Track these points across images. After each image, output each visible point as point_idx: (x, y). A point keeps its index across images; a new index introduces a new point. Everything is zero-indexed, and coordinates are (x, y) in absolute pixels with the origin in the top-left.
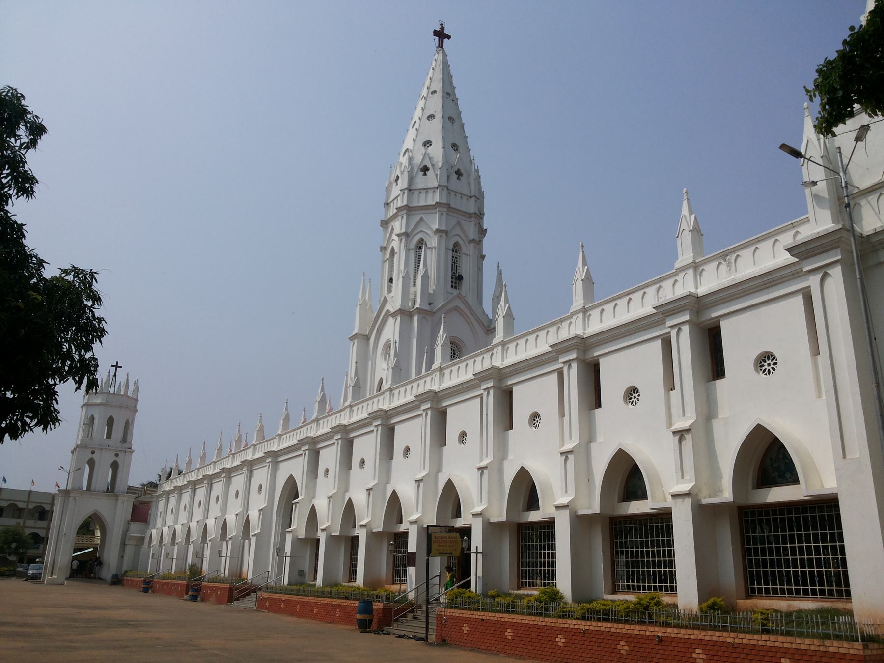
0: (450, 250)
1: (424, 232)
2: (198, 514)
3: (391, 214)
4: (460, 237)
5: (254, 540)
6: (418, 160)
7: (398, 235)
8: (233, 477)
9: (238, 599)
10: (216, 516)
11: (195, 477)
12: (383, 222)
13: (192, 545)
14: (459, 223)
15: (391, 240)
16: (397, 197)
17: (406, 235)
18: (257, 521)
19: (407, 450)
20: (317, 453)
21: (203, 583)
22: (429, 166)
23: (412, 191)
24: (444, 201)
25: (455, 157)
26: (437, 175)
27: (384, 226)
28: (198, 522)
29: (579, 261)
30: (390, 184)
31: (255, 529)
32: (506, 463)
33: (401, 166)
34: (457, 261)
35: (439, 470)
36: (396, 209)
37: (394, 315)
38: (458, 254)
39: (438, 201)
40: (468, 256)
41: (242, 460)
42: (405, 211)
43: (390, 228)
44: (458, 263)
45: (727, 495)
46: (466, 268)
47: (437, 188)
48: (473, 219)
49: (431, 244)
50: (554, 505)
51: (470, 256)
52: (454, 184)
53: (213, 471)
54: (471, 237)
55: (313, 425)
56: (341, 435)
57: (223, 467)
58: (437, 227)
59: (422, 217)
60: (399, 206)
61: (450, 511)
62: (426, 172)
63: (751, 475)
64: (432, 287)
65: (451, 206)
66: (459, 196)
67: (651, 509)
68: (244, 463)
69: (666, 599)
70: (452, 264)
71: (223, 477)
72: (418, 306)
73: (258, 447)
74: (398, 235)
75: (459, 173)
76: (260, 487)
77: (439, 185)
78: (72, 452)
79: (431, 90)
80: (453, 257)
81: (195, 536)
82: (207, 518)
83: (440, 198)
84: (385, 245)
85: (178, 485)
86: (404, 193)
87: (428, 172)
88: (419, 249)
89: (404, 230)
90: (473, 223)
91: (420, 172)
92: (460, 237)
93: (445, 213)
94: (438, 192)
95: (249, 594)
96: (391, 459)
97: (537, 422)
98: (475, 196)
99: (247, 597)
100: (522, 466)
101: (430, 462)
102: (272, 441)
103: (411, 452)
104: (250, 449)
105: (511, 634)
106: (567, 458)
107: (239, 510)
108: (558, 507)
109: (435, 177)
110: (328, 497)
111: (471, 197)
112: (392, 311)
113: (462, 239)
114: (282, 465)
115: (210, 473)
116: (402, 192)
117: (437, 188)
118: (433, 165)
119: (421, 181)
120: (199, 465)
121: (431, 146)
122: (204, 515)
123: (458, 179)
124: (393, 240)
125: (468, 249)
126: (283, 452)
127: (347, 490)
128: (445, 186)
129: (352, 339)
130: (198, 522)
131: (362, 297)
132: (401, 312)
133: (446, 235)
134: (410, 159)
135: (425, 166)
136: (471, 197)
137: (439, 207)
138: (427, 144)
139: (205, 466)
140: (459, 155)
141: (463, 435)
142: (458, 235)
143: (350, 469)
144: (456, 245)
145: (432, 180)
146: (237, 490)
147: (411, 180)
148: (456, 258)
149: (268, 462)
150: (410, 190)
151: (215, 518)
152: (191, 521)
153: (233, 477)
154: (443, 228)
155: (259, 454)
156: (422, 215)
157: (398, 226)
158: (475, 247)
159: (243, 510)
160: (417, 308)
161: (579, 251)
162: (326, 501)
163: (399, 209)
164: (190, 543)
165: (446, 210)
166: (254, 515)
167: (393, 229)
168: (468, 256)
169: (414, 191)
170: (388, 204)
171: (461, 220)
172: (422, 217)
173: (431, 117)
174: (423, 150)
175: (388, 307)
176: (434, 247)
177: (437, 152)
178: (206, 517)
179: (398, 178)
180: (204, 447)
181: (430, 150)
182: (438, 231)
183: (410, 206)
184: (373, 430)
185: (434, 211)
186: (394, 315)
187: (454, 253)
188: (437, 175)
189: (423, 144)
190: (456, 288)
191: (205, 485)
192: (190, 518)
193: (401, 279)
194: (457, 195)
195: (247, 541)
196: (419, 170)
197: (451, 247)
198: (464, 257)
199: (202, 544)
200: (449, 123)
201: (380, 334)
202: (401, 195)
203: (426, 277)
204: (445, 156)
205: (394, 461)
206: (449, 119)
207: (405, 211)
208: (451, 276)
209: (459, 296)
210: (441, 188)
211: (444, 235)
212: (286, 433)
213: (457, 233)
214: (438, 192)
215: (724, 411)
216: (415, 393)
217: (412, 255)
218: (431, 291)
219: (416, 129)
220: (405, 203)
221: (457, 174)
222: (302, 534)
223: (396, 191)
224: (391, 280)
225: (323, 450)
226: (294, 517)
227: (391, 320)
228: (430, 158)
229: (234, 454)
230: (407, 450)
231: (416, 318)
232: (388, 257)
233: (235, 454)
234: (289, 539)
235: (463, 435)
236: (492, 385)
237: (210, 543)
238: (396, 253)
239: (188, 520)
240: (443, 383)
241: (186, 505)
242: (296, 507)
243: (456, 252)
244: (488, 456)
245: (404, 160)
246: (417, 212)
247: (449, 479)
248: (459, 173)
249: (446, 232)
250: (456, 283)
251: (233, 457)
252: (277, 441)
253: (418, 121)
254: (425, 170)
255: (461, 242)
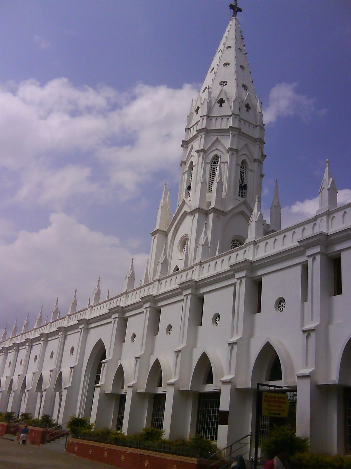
0: (239, 165)
1: (219, 150)
2: (19, 370)
3: (191, 137)
4: (247, 156)
5: (65, 393)
6: (216, 94)
7: (197, 152)
8: (68, 335)
9: (49, 442)
10: (34, 372)
11: (8, 344)
12: (184, 142)
13: (13, 393)
14: (246, 145)
15: (191, 155)
16: (197, 123)
17: (203, 151)
18: (69, 377)
19: (170, 328)
20: (158, 312)
21: (20, 425)
22: (225, 99)
23: (210, 118)
24: (236, 126)
25: (245, 96)
26: (231, 107)
27: (185, 146)
28: (19, 375)
29: (202, 234)
30: (191, 114)
31: (67, 382)
32: (252, 339)
33: (201, 100)
34: (243, 175)
35: (194, 346)
36: (196, 131)
37: (192, 213)
38: (245, 170)
39: (231, 126)
40: (253, 172)
41: (58, 326)
42: (204, 133)
43: (190, 148)
44: (244, 176)
45: (334, 377)
46: (251, 180)
47: (231, 116)
48: (258, 143)
49: (224, 160)
50: (221, 381)
51: (254, 172)
52: (245, 115)
53: (21, 340)
54: (256, 158)
55: (122, 297)
56: (118, 315)
57: (81, 318)
58: (230, 146)
59: (217, 138)
60: (198, 129)
61: (157, 382)
62: (222, 104)
63: (157, 382)
64: (224, 193)
65: (241, 131)
66: (247, 124)
67: (163, 391)
68: (60, 329)
69: (214, 443)
70: (240, 178)
71: (42, 341)
72: (213, 205)
73: (72, 316)
74: (197, 152)
75: (247, 106)
76: (72, 349)
77: (232, 114)
78: (185, 132)
79: (227, 45)
80: (241, 172)
81: (16, 386)
82: (27, 373)
83: (234, 122)
84: (185, 161)
85: (30, 338)
86: (204, 118)
87: (224, 104)
88: (214, 164)
89: (202, 148)
90: (258, 147)
91: (217, 103)
92: (247, 156)
93: (236, 136)
94: (231, 119)
95: (58, 438)
96: (123, 343)
97: (218, 320)
98: (260, 126)
99: (57, 441)
100: (268, 342)
101: (244, 330)
102: (63, 320)
103: (173, 329)
104: (65, 319)
105: (148, 463)
106: (232, 348)
107: (53, 367)
108: (300, 377)
109: (229, 107)
110: (136, 358)
111: (256, 126)
112: (189, 211)
113: (249, 158)
114: (92, 331)
115: (31, 337)
116: (202, 118)
117: (231, 116)
118: (228, 99)
119: (217, 111)
120: (23, 331)
121: (226, 85)
122: (12, 373)
123: (247, 111)
124: (192, 156)
125: (253, 166)
126: (99, 318)
127: (120, 359)
128: (237, 115)
129: (153, 234)
130: (19, 375)
131: (163, 202)
132: (198, 210)
133: (237, 154)
134: (210, 93)
135: (221, 99)
136: (256, 126)
137: (232, 130)
138: (223, 83)
139: (27, 332)
140: (248, 93)
141: (217, 317)
142: (246, 154)
143: (157, 334)
144: (244, 162)
145: (227, 109)
146: (36, 355)
147: (210, 109)
148: (243, 173)
149: (81, 329)
150: (208, 117)
151: (34, 373)
152: (27, 373)
153: (68, 335)
154: (235, 147)
155: (54, 329)
156: (218, 137)
157: (197, 145)
158: (258, 165)
159: (57, 368)
160: (213, 208)
161: (164, 247)
162: (133, 361)
163: (199, 131)
164: (12, 392)
165: (237, 133)
166: (66, 372)
167: (192, 147)
168: (253, 172)
169: (212, 118)
170: (189, 129)
171: (248, 143)
172: (217, 138)
173: (226, 64)
174: (220, 87)
175: (186, 208)
176: (226, 162)
177: (231, 90)
178: (25, 372)
179: (198, 108)
180: (57, 303)
181: (225, 87)
182: (230, 149)
183: (208, 129)
184: (143, 312)
185: (227, 134)
186: (192, 213)
187: (242, 169)
188: (231, 107)
189: (220, 83)
190: (242, 196)
191: (59, 337)
192: (13, 373)
193: (200, 184)
194: (246, 123)
195: (58, 394)
196: (217, 102)
197: (240, 163)
198: (250, 172)
199: (21, 394)
200: (240, 69)
201: (177, 231)
202: (201, 120)
203: (220, 184)
204: (238, 92)
205: (125, 344)
206: (240, 67)
207: (204, 133)
208: (239, 187)
209: (245, 203)
210: (234, 116)
211: (235, 153)
212: (97, 305)
213: (245, 153)
214: (231, 119)
215: (337, 320)
216: (108, 308)
217: (208, 167)
218: (223, 197)
219: (215, 72)
220: (204, 126)
221: (246, 107)
222: (109, 389)
223: (196, 118)
224: (189, 188)
225: (130, 318)
226: (102, 375)
227: (188, 218)
228: (226, 93)
229: (92, 307)
230: (170, 328)
231: (211, 216)
232: (187, 169)
233: (52, 322)
234: (97, 392)
235: (217, 317)
236: (149, 306)
237: (27, 393)
238: (195, 166)
239: (11, 374)
240: (160, 290)
241: (36, 356)
242: (104, 366)
243: (243, 168)
244: (183, 343)
245: (205, 95)
246: (214, 134)
247: (268, 343)
248: (247, 106)
249: (237, 151)
250: (242, 193)
251: (51, 325)
252: (67, 319)
253: (216, 67)
254: (221, 102)
255: (248, 160)
